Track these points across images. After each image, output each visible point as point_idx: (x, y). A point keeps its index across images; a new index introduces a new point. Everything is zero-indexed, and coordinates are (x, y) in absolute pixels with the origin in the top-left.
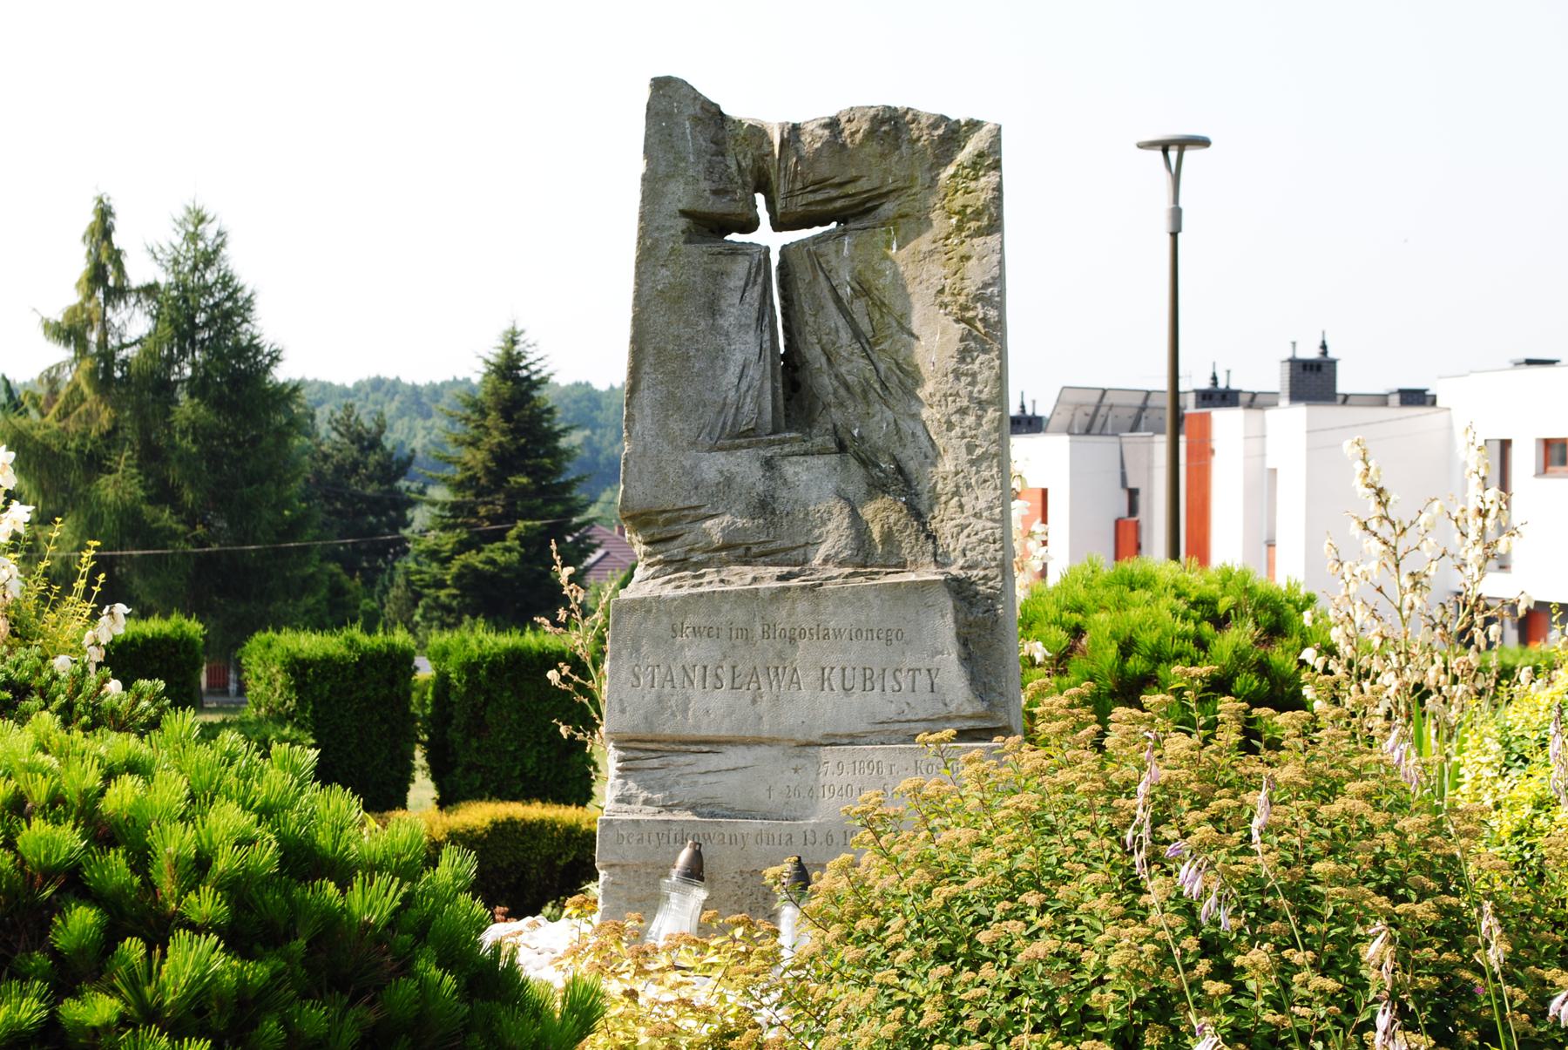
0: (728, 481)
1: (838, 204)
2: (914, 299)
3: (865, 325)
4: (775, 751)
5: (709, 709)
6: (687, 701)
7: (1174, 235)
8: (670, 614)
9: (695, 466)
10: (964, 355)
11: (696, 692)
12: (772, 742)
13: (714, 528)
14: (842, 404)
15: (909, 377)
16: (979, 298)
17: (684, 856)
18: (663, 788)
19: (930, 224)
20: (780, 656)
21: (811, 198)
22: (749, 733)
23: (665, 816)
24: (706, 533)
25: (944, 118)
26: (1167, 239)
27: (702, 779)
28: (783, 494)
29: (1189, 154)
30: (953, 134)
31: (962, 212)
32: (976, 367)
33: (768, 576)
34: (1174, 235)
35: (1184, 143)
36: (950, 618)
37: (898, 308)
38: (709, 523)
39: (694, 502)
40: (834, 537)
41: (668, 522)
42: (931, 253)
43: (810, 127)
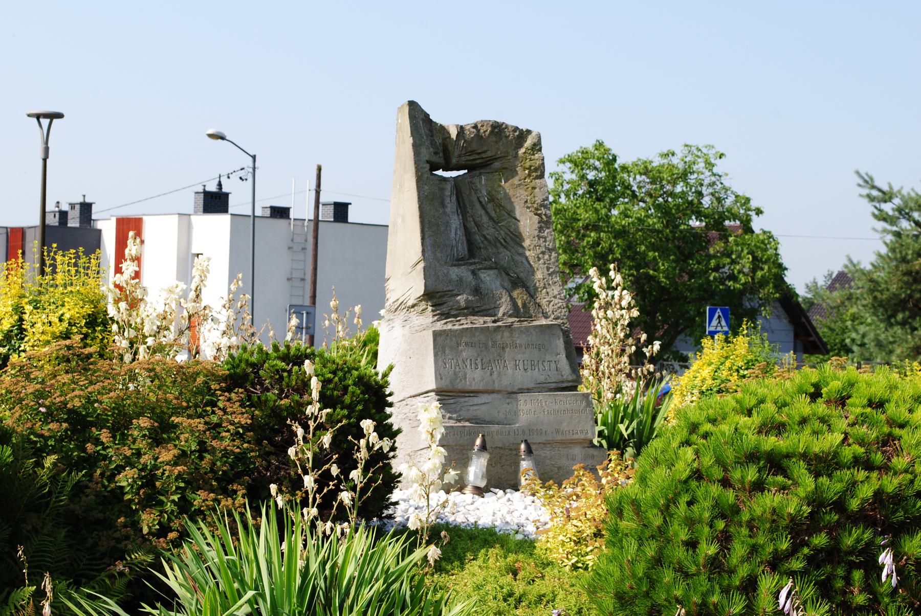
0: (461, 280)
1: (478, 161)
2: (515, 204)
3: (493, 214)
4: (499, 396)
5: (474, 377)
6: (465, 374)
7: (45, 160)
8: (455, 336)
9: (448, 273)
10: (541, 229)
11: (468, 370)
12: (498, 392)
13: (462, 299)
14: (486, 248)
15: (517, 239)
16: (542, 205)
17: (478, 442)
18: (456, 412)
19: (517, 173)
20: (499, 355)
21: (468, 158)
22: (490, 388)
23: (459, 424)
24: (458, 302)
25: (517, 128)
26: (41, 162)
27: (471, 408)
28: (482, 285)
29: (55, 121)
30: (523, 135)
31: (529, 168)
32: (545, 234)
33: (479, 322)
34: (45, 160)
35: (54, 116)
36: (562, 340)
37: (508, 207)
38: (459, 298)
39: (451, 288)
40: (504, 307)
41: (441, 297)
42: (520, 185)
43: (468, 127)
